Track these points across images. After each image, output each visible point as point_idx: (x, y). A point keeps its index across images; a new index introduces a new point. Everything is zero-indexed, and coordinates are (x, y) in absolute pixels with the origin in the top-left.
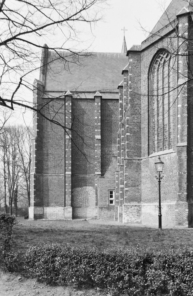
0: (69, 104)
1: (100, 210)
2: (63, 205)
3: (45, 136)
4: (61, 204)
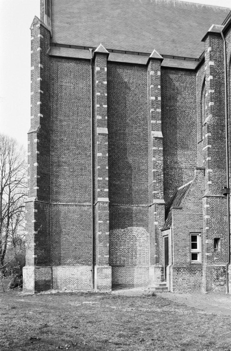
0: (100, 67)
1: (176, 273)
2: (89, 263)
3: (55, 128)
4: (85, 261)
